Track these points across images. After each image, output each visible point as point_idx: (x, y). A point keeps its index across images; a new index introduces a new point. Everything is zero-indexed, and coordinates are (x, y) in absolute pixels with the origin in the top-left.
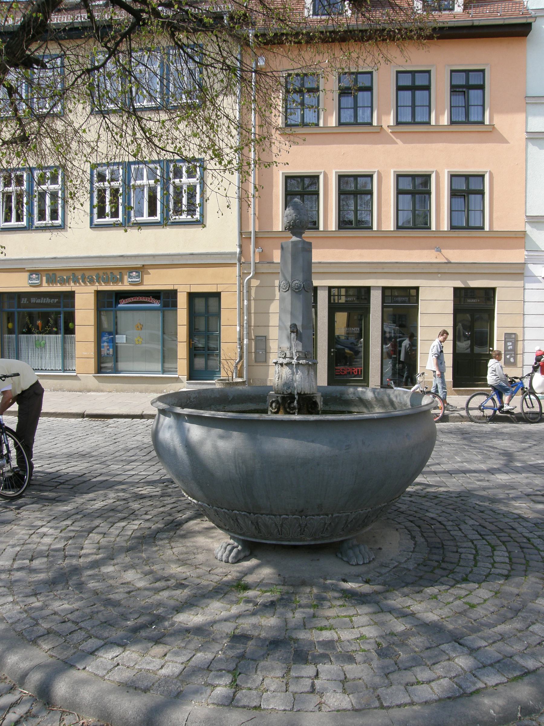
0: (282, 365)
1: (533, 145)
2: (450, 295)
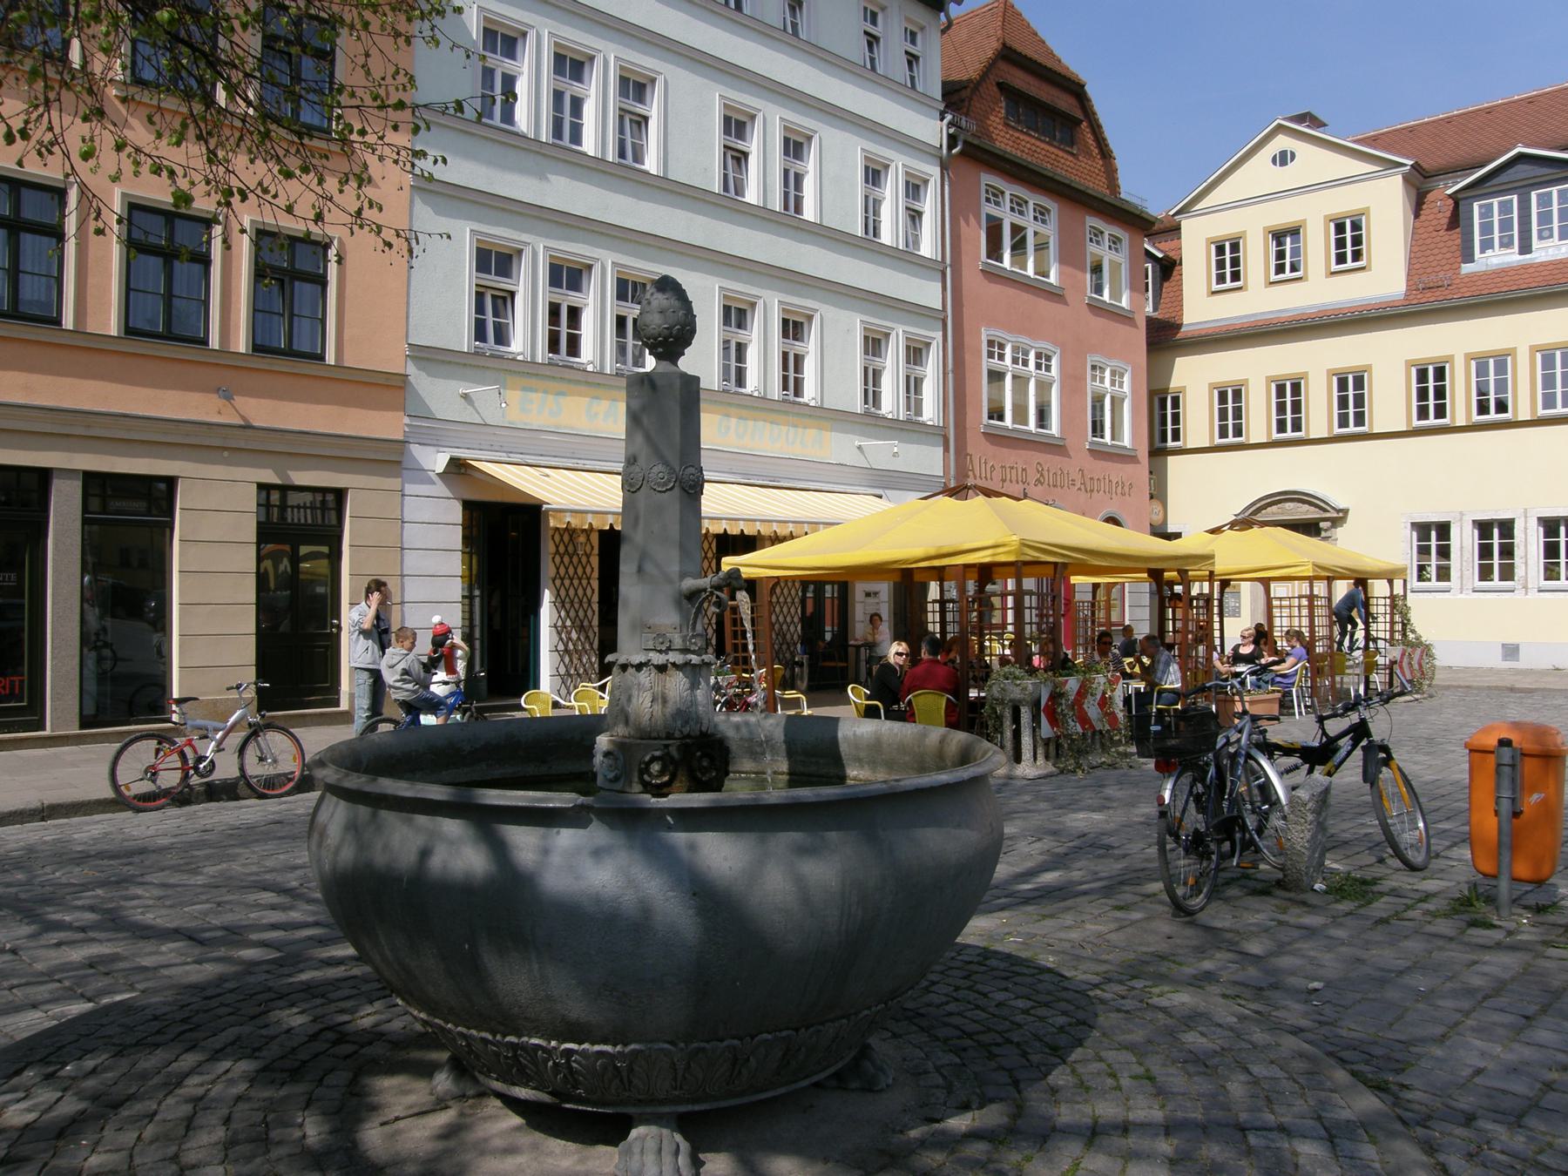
0: (661, 669)
1: (425, 202)
2: (249, 500)
